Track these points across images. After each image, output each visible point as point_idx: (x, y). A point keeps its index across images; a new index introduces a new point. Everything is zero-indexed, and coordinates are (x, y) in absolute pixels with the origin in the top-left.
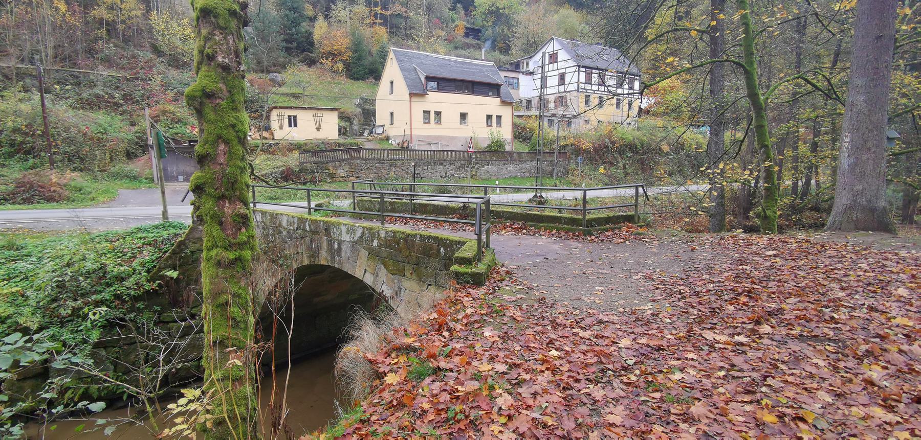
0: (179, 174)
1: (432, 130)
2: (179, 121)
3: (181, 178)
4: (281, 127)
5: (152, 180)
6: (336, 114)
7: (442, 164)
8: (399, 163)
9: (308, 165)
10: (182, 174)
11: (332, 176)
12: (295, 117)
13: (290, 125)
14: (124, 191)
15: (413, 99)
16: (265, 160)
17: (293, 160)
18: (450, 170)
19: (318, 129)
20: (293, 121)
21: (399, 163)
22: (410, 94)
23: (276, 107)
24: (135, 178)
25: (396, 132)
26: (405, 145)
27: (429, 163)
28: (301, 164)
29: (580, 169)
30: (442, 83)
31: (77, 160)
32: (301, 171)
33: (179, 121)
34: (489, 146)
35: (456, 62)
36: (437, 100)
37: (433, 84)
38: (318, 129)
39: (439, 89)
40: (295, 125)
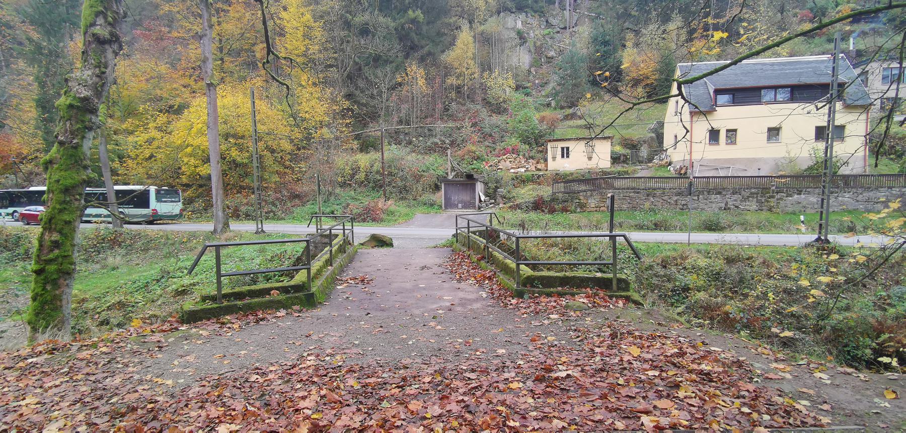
0: (459, 202)
1: (722, 151)
2: (478, 158)
3: (460, 205)
4: (554, 158)
5: (441, 206)
6: (825, 124)
7: (720, 193)
8: (658, 192)
9: (560, 195)
10: (461, 202)
11: (582, 206)
12: (568, 149)
13: (563, 156)
14: (420, 215)
15: (695, 119)
16: (529, 190)
17: (546, 191)
18: (732, 200)
19: (590, 158)
20: (565, 153)
21: (658, 192)
22: (691, 113)
23: (550, 141)
24: (432, 205)
25: (677, 155)
26: (683, 172)
27: (702, 192)
28: (554, 193)
29: (598, 216)
30: (739, 95)
31: (403, 192)
32: (553, 200)
33: (478, 158)
34: (810, 168)
35: (773, 64)
36: (727, 116)
37: (723, 99)
38: (590, 158)
39: (735, 102)
40: (568, 157)
